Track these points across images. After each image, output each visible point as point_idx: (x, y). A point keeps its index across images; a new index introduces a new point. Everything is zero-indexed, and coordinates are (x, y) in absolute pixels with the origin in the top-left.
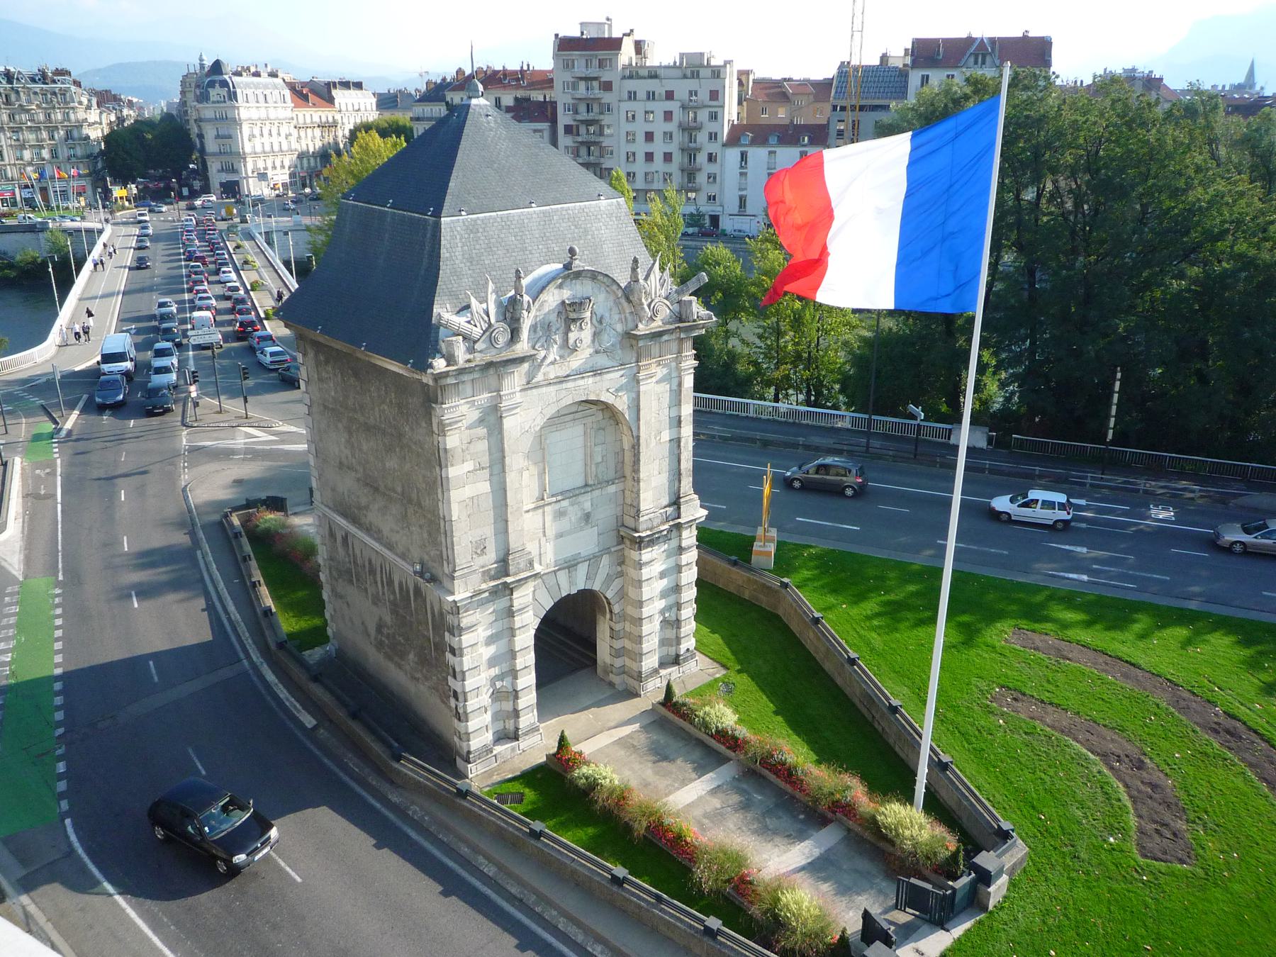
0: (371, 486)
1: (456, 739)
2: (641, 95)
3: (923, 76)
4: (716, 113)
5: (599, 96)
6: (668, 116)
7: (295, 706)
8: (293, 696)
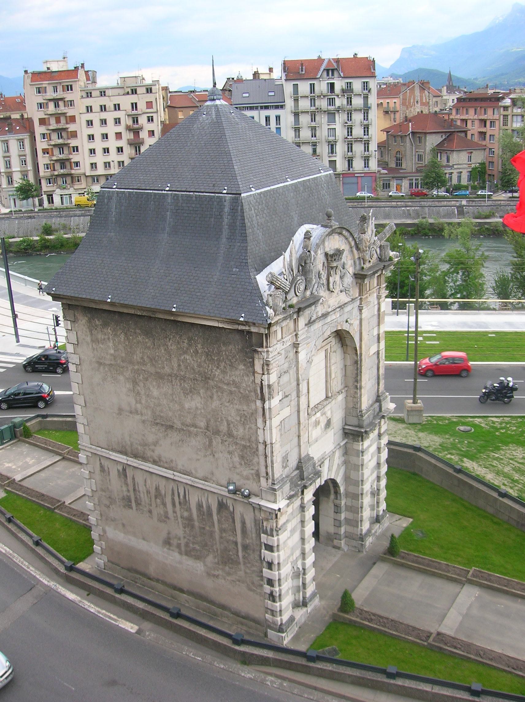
0: (162, 425)
1: (268, 616)
2: (96, 108)
3: (311, 84)
4: (152, 117)
5: (65, 111)
6: (117, 121)
7: (110, 617)
8: (103, 609)
